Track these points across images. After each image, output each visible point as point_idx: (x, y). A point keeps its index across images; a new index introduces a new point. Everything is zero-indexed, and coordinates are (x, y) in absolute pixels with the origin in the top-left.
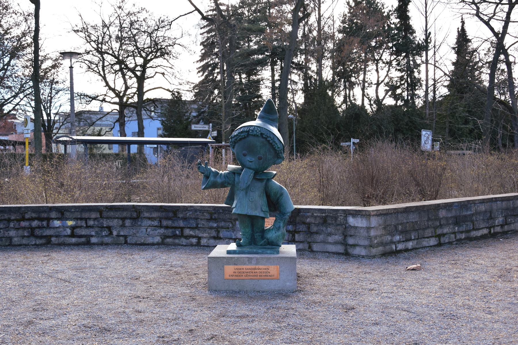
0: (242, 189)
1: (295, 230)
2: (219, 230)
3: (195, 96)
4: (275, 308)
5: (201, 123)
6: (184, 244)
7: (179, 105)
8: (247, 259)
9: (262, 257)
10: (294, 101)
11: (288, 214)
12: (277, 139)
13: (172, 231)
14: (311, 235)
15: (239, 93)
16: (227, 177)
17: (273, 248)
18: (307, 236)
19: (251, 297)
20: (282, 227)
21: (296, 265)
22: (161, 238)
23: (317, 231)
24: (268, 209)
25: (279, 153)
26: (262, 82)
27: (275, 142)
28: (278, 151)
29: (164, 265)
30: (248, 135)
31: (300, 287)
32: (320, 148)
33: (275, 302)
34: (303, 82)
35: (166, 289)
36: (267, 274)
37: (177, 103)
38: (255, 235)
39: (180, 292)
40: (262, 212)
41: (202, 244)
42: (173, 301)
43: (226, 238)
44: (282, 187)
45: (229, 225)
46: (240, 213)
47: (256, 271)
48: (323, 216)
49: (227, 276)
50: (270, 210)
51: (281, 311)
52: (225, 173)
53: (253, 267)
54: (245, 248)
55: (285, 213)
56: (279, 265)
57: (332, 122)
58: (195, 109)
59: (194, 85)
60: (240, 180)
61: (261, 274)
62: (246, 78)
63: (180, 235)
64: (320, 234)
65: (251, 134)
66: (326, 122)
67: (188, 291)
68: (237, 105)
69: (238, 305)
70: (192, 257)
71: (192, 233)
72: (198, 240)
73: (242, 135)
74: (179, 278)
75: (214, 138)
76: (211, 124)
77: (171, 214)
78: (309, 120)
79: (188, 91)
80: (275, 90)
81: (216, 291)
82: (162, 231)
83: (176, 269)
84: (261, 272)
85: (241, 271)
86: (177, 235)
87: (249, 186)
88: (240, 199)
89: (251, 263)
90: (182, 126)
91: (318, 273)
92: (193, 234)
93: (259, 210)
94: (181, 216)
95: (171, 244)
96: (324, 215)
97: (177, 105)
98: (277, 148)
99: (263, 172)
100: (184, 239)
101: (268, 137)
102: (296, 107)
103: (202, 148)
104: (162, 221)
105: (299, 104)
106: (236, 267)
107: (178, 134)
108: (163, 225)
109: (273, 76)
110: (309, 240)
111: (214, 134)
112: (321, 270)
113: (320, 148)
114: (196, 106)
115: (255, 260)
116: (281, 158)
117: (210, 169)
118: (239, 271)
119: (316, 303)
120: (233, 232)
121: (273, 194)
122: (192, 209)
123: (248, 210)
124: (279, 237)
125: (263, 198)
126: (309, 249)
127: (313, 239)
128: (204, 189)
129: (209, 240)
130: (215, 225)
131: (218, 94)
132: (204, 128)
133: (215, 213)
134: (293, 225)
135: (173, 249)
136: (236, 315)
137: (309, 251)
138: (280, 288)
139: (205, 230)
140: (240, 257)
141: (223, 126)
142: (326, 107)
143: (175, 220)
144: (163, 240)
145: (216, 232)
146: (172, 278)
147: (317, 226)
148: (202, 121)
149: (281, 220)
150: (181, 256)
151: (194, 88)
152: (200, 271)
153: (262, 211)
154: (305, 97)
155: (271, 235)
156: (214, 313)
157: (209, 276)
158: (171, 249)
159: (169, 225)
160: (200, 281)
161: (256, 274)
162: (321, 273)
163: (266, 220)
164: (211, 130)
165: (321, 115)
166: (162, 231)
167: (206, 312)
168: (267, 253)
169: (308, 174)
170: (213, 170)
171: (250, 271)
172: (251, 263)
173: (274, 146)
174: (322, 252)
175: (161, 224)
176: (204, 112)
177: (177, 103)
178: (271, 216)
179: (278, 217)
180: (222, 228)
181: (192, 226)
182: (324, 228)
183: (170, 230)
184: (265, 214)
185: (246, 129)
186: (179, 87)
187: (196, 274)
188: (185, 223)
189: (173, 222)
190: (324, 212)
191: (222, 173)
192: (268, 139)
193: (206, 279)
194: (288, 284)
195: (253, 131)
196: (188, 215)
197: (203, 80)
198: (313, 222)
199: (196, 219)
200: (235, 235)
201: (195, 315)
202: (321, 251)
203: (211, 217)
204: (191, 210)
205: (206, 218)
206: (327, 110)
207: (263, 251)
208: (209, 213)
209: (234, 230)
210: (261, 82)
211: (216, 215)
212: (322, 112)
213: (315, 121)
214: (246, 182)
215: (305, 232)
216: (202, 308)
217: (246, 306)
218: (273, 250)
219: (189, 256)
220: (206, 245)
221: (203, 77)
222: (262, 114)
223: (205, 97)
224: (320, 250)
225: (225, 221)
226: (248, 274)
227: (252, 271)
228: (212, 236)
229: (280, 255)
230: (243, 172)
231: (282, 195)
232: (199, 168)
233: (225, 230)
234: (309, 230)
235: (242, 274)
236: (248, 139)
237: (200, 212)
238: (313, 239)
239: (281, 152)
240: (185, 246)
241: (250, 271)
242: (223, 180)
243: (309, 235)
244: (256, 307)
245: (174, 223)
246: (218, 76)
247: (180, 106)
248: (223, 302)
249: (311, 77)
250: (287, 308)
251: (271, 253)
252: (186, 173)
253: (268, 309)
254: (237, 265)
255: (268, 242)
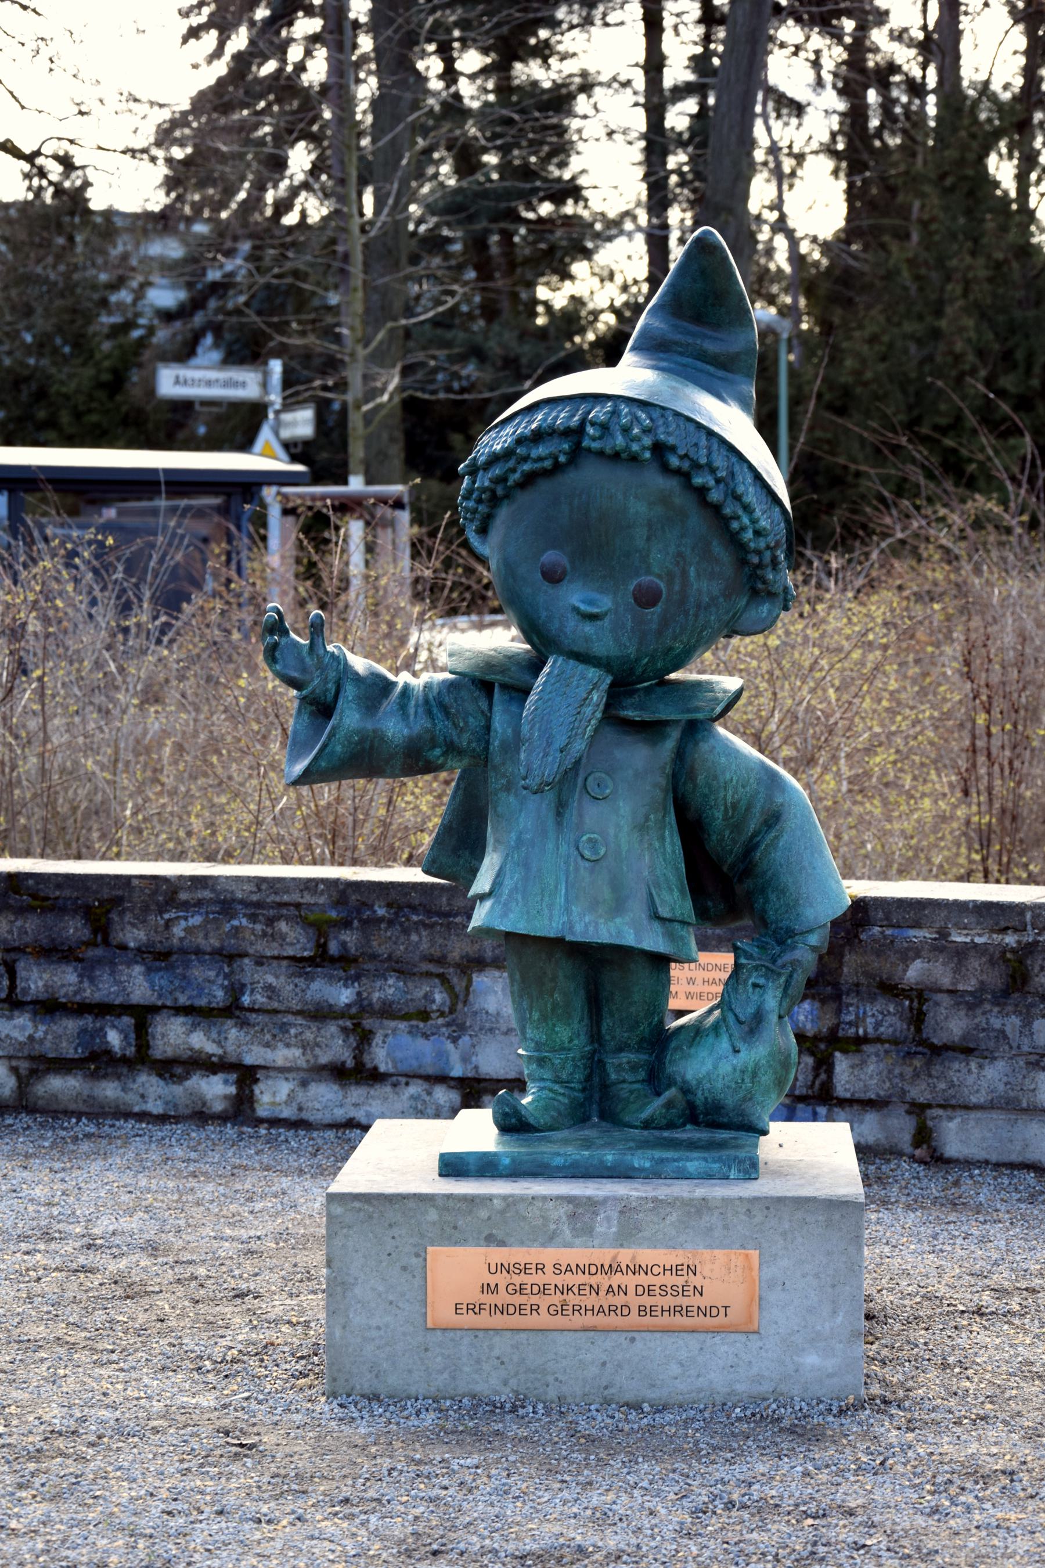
0: (533, 782)
1: (834, 1030)
2: (368, 1023)
3: (170, 184)
4: (744, 1507)
5: (208, 353)
6: (155, 1107)
7: (71, 239)
8: (563, 1211)
9: (655, 1200)
10: (781, 226)
11: (813, 939)
12: (749, 480)
13: (83, 1031)
14: (929, 1064)
15: (445, 169)
16: (445, 709)
17: (721, 1145)
18: (908, 1071)
19: (591, 1440)
20: (774, 1018)
21: (860, 1250)
22: (15, 1070)
23: (964, 1037)
24: (689, 904)
25: (760, 566)
26: (582, 98)
27: (738, 498)
28: (758, 552)
29: (47, 1236)
30: (577, 453)
31: (884, 1382)
32: (956, 519)
33: (739, 1470)
34: (842, 106)
35: (70, 1385)
36: (685, 1302)
37: (59, 227)
38: (611, 1061)
39: (157, 1406)
40: (656, 925)
41: (262, 1112)
42: (125, 1459)
43: (411, 1076)
44: (774, 776)
45: (428, 998)
46: (522, 928)
47: (617, 1279)
48: (1004, 950)
49: (441, 1312)
50: (702, 913)
51: (779, 1528)
52: (428, 686)
53: (604, 1255)
54: (549, 1141)
55: (791, 933)
56: (758, 1247)
57: (1019, 355)
58: (168, 267)
59: (166, 115)
60: (525, 729)
61: (647, 1301)
62: (485, 71)
63: (131, 1051)
64: (988, 1056)
65: (595, 445)
66: (981, 353)
67: (208, 1400)
68: (434, 243)
69: (516, 1484)
70: (207, 1190)
71: (200, 1041)
72: (240, 1083)
73: (541, 450)
74: (142, 1318)
75: (295, 450)
76: (276, 366)
77: (74, 929)
78: (873, 340)
79: (132, 152)
80: (665, 153)
81: (374, 1397)
82: (23, 1028)
83: (123, 1264)
84: (649, 1291)
85: (528, 1279)
86: (108, 1052)
87: (578, 763)
88: (520, 842)
89: (588, 1231)
90: (89, 372)
91: (986, 1298)
92: (211, 1048)
93: (637, 909)
94: (134, 936)
95: (72, 1107)
96: (1010, 939)
97: (61, 241)
98: (749, 535)
99: (663, 683)
100: (154, 1079)
101: (697, 466)
102: (797, 259)
103: (224, 511)
104: (20, 965)
105: (814, 240)
106: (498, 1255)
107: (65, 418)
108: (26, 991)
109: (654, 64)
110: (919, 1092)
111: (294, 424)
112: (1002, 1277)
113: (956, 519)
114: (171, 249)
115: (615, 1215)
116: (771, 595)
117: (338, 660)
118: (517, 1280)
119: (986, 1479)
120: (455, 1040)
121: (719, 815)
122: (207, 894)
123: (568, 911)
124: (754, 1075)
125: (662, 839)
126: (917, 1144)
127: (942, 1086)
128: (307, 778)
129: (304, 1084)
130: (344, 996)
131: (315, 170)
132: (236, 384)
133: (346, 924)
134: (823, 1001)
135: (88, 1136)
136: (511, 1547)
137: (921, 1162)
138: (766, 1387)
139: (284, 1028)
140: (522, 1199)
141: (355, 376)
142: (981, 261)
143: (99, 962)
144: (24, 1082)
145: (353, 1041)
146: (99, 1316)
147: (971, 1007)
148: (209, 340)
149: (771, 973)
150: (143, 1182)
151: (165, 136)
152: (266, 1275)
153: (656, 917)
154: (851, 194)
155: (709, 1066)
156: (375, 1534)
157: (332, 1312)
158: (75, 1139)
159: (63, 995)
160: (270, 1335)
161: (619, 1300)
162: (1000, 1292)
163: (676, 971)
164: (275, 398)
165: (949, 310)
166: (23, 1028)
167: (328, 1527)
168: (683, 1176)
169: (893, 685)
170: (359, 664)
171: (581, 1279)
172: (588, 1231)
173: (735, 525)
174: (998, 1166)
175: (12, 987)
176: (220, 288)
177: (59, 227)
178: (704, 945)
179: (750, 957)
180: (388, 1011)
181: (202, 1002)
182: (1013, 1023)
183: (71, 1025)
184: (671, 936)
185: (561, 417)
186: (75, 127)
187: (241, 1295)
188: (161, 980)
189: (88, 971)
190: (1015, 922)
191: (414, 682)
192: (698, 480)
193: (307, 1324)
194: (811, 1359)
195: (604, 428)
196: (178, 931)
197: (221, 82)
198: (946, 981)
199: (229, 957)
200: (465, 1059)
201: (266, 1548)
202: (994, 1158)
203: (322, 947)
204: (199, 903)
205: (290, 952)
206: (990, 280)
207: (662, 1161)
208: (307, 923)
209: (458, 1029)
210: (582, 104)
211: (350, 938)
212: (959, 290)
213: (913, 348)
214: (560, 741)
215: (895, 1042)
216: (299, 1505)
217: (565, 1494)
218: (725, 1153)
219: (192, 1183)
220: (286, 1113)
221: (221, 68)
222: (657, 324)
223: (230, 192)
224: (982, 1155)
225: (403, 970)
226: (572, 1299)
227: (594, 1280)
228: (324, 1059)
229: (762, 1187)
230: (541, 679)
231: (773, 819)
232: (272, 654)
233: (402, 1025)
234: (919, 1030)
235: (534, 1299)
236: (572, 478)
237: (253, 918)
238: (942, 1086)
239: (775, 563)
240: (162, 1119)
241: (581, 1279)
242: (417, 729)
243: (917, 1063)
244: (624, 1498)
245: (92, 980)
246: (309, 64)
247: (79, 249)
248: (426, 1469)
249: (893, 68)
250: (813, 1507)
251: (708, 1176)
252: (141, 670)
253: (699, 1512)
254: (502, 1243)
255: (691, 1106)
